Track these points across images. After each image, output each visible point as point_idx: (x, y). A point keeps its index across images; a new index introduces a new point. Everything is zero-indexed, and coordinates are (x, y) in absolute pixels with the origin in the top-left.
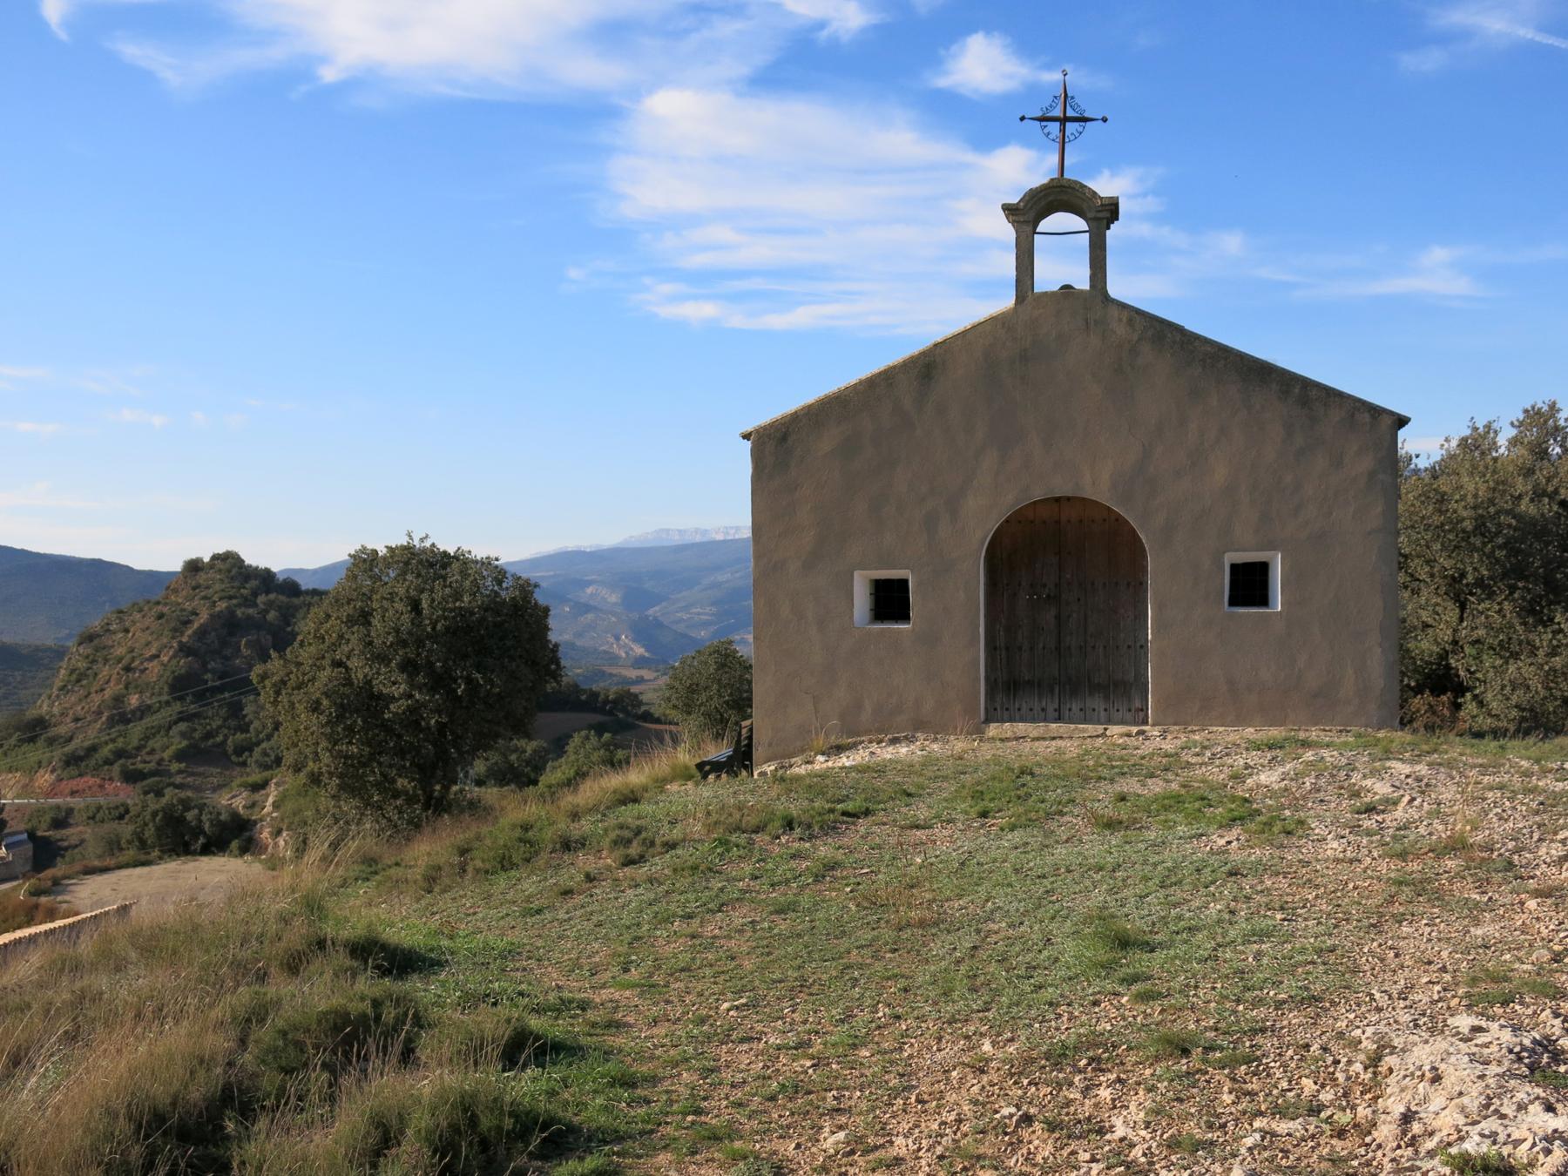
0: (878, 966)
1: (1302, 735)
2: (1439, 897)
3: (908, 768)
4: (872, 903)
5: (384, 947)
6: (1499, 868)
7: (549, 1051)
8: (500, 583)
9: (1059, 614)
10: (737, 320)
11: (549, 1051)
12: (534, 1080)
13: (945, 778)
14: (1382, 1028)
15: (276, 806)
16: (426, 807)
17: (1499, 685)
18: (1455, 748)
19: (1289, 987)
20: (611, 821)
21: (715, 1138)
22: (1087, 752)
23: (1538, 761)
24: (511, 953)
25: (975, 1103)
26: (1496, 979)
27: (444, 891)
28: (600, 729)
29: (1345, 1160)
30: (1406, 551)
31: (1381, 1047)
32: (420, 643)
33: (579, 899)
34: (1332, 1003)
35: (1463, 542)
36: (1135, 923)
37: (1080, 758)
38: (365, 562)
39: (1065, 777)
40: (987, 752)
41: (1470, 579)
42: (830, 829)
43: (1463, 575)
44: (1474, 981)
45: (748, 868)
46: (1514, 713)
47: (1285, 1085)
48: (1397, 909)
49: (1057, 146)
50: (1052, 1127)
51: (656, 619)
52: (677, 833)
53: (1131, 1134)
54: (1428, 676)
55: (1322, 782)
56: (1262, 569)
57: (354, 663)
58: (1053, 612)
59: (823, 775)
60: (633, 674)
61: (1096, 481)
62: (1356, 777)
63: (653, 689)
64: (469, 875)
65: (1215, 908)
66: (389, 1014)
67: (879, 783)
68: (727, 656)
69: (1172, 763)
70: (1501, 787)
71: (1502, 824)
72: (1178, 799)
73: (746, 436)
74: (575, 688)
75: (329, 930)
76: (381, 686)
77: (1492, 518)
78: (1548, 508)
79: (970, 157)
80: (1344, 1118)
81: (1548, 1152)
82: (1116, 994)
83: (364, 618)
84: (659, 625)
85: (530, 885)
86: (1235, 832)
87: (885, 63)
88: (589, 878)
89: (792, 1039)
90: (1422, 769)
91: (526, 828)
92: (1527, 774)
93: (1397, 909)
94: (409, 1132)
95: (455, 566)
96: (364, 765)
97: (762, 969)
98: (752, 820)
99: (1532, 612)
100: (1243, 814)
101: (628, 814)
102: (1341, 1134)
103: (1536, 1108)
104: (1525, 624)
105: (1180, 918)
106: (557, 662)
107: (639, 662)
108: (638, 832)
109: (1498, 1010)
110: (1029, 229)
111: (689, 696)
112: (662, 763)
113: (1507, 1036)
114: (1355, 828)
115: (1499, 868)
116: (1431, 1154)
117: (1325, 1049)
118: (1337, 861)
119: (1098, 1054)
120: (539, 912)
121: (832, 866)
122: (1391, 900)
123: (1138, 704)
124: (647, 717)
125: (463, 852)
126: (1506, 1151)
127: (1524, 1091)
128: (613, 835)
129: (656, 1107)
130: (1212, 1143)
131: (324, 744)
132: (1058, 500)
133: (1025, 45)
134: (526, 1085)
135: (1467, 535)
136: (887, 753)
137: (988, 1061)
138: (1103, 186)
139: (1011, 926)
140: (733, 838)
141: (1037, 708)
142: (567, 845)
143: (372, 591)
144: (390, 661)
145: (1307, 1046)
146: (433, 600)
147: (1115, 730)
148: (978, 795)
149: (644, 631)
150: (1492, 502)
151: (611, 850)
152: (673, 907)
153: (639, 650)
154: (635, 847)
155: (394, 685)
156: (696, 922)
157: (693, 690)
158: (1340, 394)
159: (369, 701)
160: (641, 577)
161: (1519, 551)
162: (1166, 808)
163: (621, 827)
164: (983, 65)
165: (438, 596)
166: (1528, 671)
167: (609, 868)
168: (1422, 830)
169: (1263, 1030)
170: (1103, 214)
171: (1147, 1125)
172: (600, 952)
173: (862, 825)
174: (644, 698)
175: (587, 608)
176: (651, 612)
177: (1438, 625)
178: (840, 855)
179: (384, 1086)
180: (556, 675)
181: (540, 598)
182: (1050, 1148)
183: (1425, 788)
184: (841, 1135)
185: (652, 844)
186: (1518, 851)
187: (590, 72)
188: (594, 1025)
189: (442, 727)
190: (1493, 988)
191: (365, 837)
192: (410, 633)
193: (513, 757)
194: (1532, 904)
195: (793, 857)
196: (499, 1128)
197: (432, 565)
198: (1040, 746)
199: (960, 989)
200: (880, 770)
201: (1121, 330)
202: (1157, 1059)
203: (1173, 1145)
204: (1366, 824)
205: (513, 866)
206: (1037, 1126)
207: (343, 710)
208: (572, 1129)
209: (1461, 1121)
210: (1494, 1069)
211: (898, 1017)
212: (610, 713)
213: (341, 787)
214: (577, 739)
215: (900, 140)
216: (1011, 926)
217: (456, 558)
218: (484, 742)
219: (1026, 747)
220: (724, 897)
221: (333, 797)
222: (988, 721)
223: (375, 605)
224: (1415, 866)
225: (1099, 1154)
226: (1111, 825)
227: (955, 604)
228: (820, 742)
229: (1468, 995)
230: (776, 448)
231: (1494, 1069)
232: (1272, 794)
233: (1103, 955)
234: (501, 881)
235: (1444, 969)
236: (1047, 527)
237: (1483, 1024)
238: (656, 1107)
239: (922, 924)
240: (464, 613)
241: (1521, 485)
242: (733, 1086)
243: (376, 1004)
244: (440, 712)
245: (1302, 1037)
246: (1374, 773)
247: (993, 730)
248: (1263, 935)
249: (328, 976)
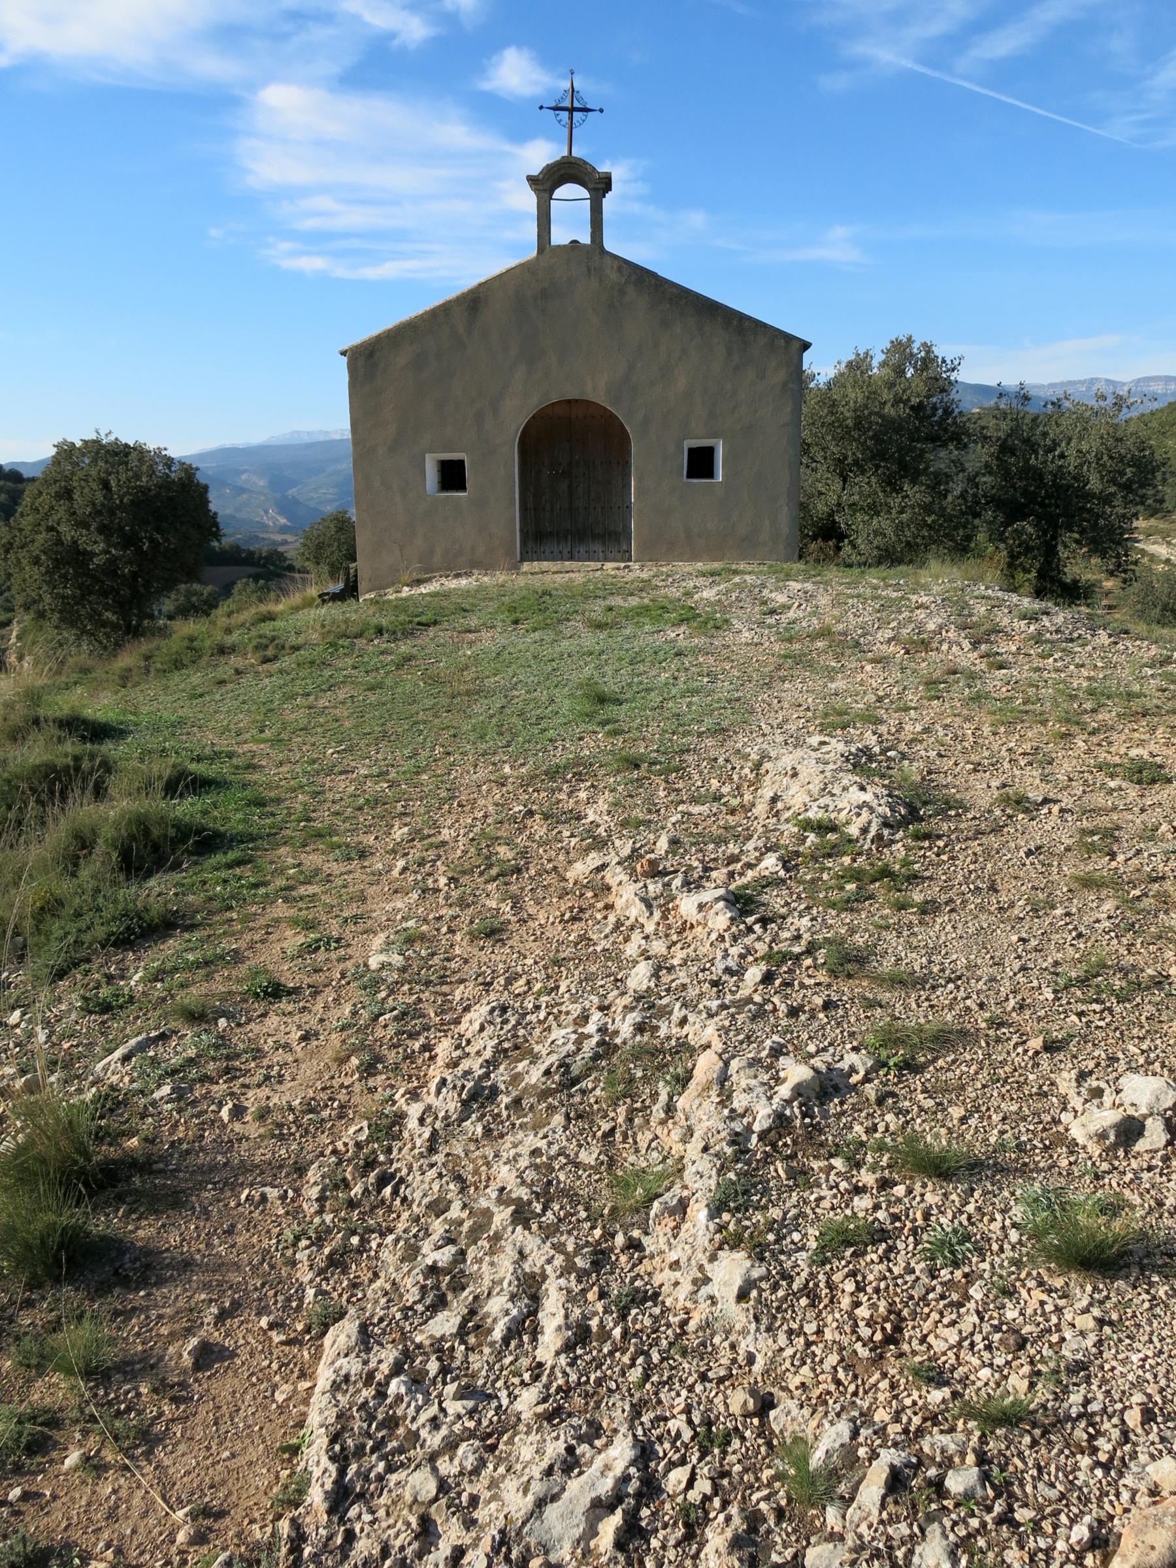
0: (436, 721)
1: (734, 567)
2: (810, 665)
3: (467, 593)
4: (434, 680)
5: (85, 722)
6: (849, 645)
7: (201, 785)
8: (169, 468)
9: (570, 484)
10: (341, 272)
11: (201, 785)
12: (192, 805)
13: (491, 599)
14: (765, 746)
15: (19, 638)
16: (128, 632)
17: (866, 532)
18: (832, 573)
19: (708, 722)
20: (254, 633)
21: (319, 835)
22: (589, 581)
23: (884, 579)
24: (181, 722)
25: (497, 805)
26: (840, 714)
27: (134, 686)
28: (256, 578)
29: (734, 827)
30: (809, 441)
31: (763, 757)
32: (112, 512)
33: (230, 686)
34: (735, 733)
35: (845, 434)
36: (610, 687)
37: (585, 584)
38: (66, 452)
39: (573, 597)
40: (521, 581)
41: (850, 460)
42: (408, 634)
43: (846, 458)
44: (826, 715)
45: (350, 661)
46: (875, 552)
47: (699, 783)
48: (782, 673)
49: (566, 131)
50: (546, 817)
52: (301, 640)
53: (598, 819)
54: (821, 528)
55: (743, 596)
56: (709, 452)
57: (63, 528)
59: (406, 599)
60: (279, 538)
62: (765, 592)
63: (293, 548)
64: (152, 674)
65: (664, 676)
66: (85, 765)
67: (444, 604)
69: (645, 586)
70: (858, 596)
71: (857, 618)
72: (647, 609)
73: (343, 353)
74: (236, 549)
75: (41, 712)
77: (866, 418)
78: (903, 411)
79: (508, 147)
80: (735, 802)
81: (858, 815)
82: (595, 732)
83: (66, 494)
84: (297, 502)
85: (196, 679)
86: (683, 628)
87: (443, 67)
88: (238, 672)
89: (375, 770)
90: (809, 586)
91: (192, 639)
92: (876, 588)
93: (782, 673)
94: (100, 841)
95: (134, 455)
96: (77, 604)
97: (356, 727)
98: (354, 630)
99: (889, 483)
100: (689, 616)
101: (267, 628)
102: (732, 812)
103: (855, 788)
104: (884, 491)
105: (641, 683)
106: (216, 525)
107: (283, 530)
108: (273, 639)
109: (839, 732)
110: (546, 195)
111: (317, 551)
112: (296, 599)
113: (841, 747)
114: (761, 624)
115: (849, 645)
116: (787, 821)
117: (727, 761)
118: (747, 644)
119: (580, 770)
120: (201, 696)
121: (409, 658)
122: (779, 668)
124: (291, 568)
125: (147, 658)
126: (833, 816)
127: (847, 779)
128: (254, 642)
129: (279, 818)
130: (650, 821)
131: (45, 588)
132: (569, 401)
133: (547, 58)
134: (187, 808)
135: (848, 431)
136: (452, 584)
137: (506, 778)
139: (528, 692)
140: (340, 642)
141: (556, 551)
142: (222, 651)
143: (73, 474)
145: (716, 759)
147: (609, 565)
148: (512, 609)
149: (286, 506)
150: (866, 406)
151: (254, 653)
152: (296, 689)
153: (283, 521)
154: (270, 650)
155: (96, 545)
156: (312, 698)
157: (320, 546)
158: (765, 325)
159: (75, 557)
160: (281, 466)
161: (883, 441)
162: (638, 615)
163: (260, 637)
164: (517, 74)
165: (123, 477)
166: (885, 524)
167: (252, 665)
168: (804, 624)
169: (688, 751)
170: (600, 186)
171: (609, 813)
172: (243, 720)
173: (432, 631)
174: (288, 555)
175: (242, 490)
176: (290, 492)
177: (828, 493)
178: (414, 651)
179: (83, 811)
180: (217, 536)
181: (200, 478)
182: (544, 830)
183: (808, 597)
184: (406, 829)
185: (283, 647)
186: (864, 635)
187: (212, 67)
188: (237, 767)
189: (134, 575)
190: (837, 719)
191: (82, 653)
193: (194, 599)
194: (868, 668)
195: (382, 653)
196: (165, 836)
197: (116, 454)
198: (558, 577)
199: (491, 733)
200: (446, 595)
201: (613, 276)
202: (619, 771)
203: (624, 824)
204: (768, 621)
205: (184, 666)
206: (537, 817)
207: (58, 563)
208: (217, 835)
209: (807, 799)
210: (831, 766)
211: (449, 754)
212: (264, 566)
213: (61, 620)
214: (239, 585)
215: (456, 133)
216: (528, 692)
217: (134, 449)
218: (168, 586)
219: (548, 578)
220: (332, 681)
221: (56, 627)
222: (522, 560)
223: (75, 484)
224: (798, 646)
225: (576, 832)
226: (600, 626)
227: (498, 479)
228: (406, 578)
229: (821, 724)
230: (366, 362)
231: (831, 766)
232: (710, 603)
233: (588, 708)
234: (176, 677)
235: (808, 709)
236: (563, 419)
237: (827, 739)
238: (279, 818)
239: (468, 693)
240: (144, 490)
241: (886, 395)
242: (333, 802)
243: (77, 759)
244: (131, 563)
245: (713, 753)
246: (778, 589)
247: (526, 567)
248: (695, 692)
249: (41, 743)
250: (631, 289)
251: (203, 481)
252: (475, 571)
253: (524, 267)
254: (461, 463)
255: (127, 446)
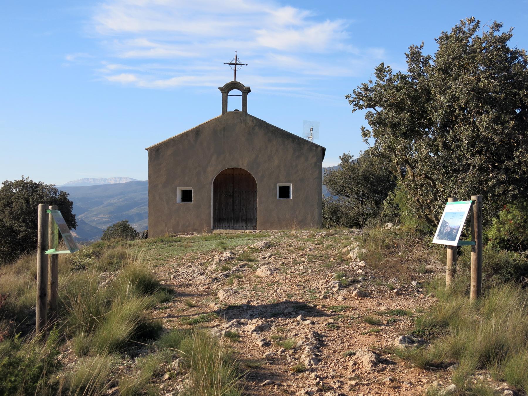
8: (56, 193)
49: (234, 71)
51: (82, 220)
58: (232, 199)
61: (244, 164)
68: (125, 227)
73: (147, 150)
76: (16, 227)
83: (9, 204)
123: (254, 225)
132: (233, 169)
138: (246, 84)
141: (227, 225)
144: (19, 219)
146: (33, 199)
147: (247, 231)
160: (102, 193)
165: (35, 197)
170: (246, 91)
181: (70, 198)
192: (26, 209)
201: (250, 123)
222: (213, 229)
223: (13, 200)
230: (156, 153)
247: (215, 231)
250: (257, 128)
251: (70, 200)
252: (195, 233)
253: (216, 119)
254: (190, 191)
255: (35, 184)
